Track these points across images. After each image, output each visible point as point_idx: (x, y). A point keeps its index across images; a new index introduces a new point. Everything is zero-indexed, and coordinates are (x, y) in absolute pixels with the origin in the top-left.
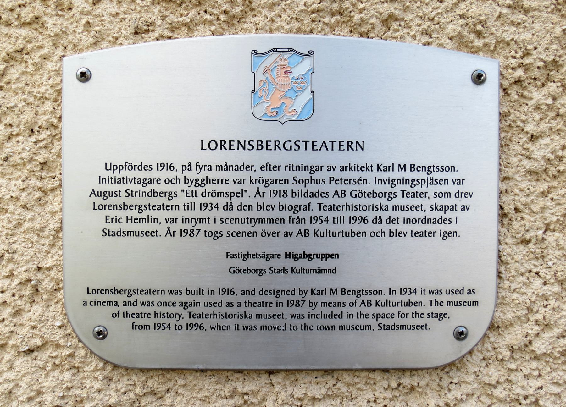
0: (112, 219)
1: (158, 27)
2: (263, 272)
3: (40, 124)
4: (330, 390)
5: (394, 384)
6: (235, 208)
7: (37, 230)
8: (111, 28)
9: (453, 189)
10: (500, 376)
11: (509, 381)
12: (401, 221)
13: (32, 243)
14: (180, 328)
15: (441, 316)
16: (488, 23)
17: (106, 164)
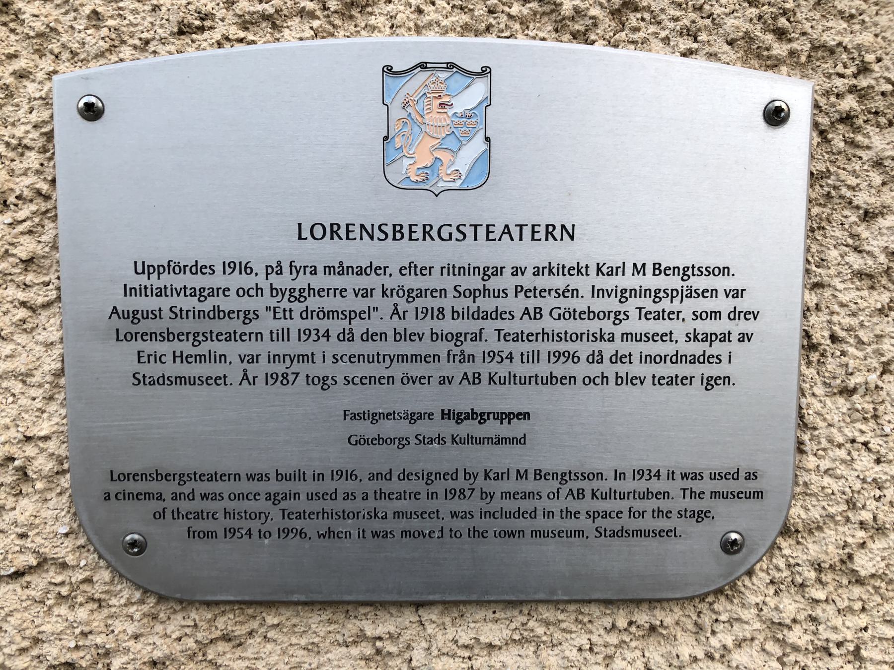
0: (149, 356)
1: (220, 23)
2: (404, 442)
3: (18, 193)
4: (517, 632)
5: (622, 623)
6: (357, 337)
7: (22, 374)
8: (134, 21)
9: (724, 305)
10: (799, 610)
11: (813, 619)
12: (635, 358)
13: (14, 395)
14: (267, 535)
15: (700, 516)
16: (799, 14)
17: (136, 263)
